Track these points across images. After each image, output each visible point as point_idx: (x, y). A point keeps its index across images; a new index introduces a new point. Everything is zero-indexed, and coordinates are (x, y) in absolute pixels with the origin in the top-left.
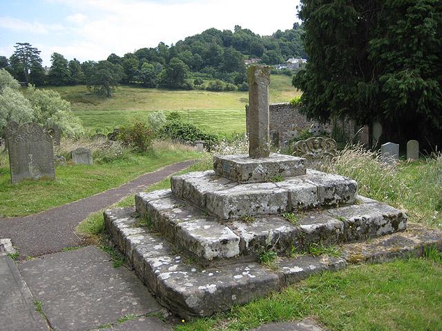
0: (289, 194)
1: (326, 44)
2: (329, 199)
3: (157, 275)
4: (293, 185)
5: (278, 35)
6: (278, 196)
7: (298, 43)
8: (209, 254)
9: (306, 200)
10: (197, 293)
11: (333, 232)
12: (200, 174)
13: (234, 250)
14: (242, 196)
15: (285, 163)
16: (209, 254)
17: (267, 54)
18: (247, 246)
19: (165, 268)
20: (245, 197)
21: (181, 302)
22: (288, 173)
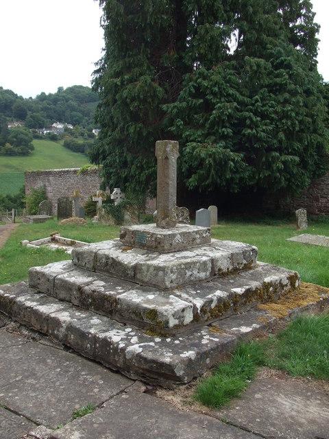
0: (213, 261)
1: (164, 113)
2: (241, 266)
3: (123, 350)
4: (202, 255)
5: (42, 97)
6: (205, 263)
7: (92, 107)
8: (173, 322)
9: (225, 265)
10: (182, 361)
11: (255, 292)
12: (111, 242)
13: (189, 317)
14: (180, 265)
15: (197, 232)
16: (173, 322)
17: (31, 117)
18: (199, 311)
19: (127, 340)
20: (183, 266)
21: (167, 372)
22: (198, 241)
